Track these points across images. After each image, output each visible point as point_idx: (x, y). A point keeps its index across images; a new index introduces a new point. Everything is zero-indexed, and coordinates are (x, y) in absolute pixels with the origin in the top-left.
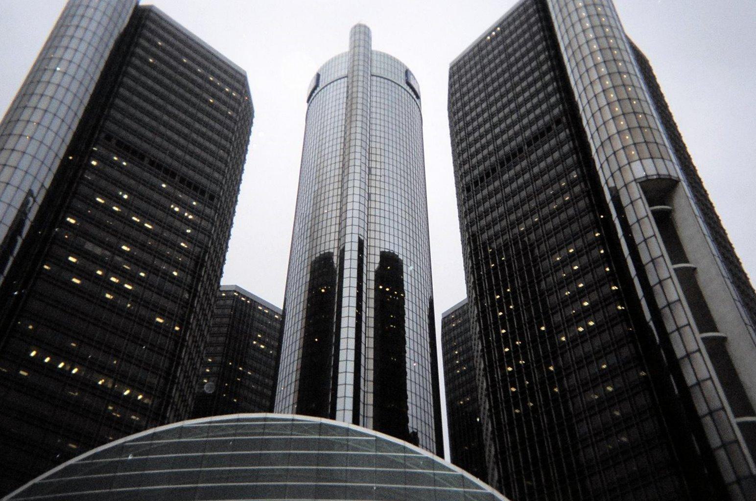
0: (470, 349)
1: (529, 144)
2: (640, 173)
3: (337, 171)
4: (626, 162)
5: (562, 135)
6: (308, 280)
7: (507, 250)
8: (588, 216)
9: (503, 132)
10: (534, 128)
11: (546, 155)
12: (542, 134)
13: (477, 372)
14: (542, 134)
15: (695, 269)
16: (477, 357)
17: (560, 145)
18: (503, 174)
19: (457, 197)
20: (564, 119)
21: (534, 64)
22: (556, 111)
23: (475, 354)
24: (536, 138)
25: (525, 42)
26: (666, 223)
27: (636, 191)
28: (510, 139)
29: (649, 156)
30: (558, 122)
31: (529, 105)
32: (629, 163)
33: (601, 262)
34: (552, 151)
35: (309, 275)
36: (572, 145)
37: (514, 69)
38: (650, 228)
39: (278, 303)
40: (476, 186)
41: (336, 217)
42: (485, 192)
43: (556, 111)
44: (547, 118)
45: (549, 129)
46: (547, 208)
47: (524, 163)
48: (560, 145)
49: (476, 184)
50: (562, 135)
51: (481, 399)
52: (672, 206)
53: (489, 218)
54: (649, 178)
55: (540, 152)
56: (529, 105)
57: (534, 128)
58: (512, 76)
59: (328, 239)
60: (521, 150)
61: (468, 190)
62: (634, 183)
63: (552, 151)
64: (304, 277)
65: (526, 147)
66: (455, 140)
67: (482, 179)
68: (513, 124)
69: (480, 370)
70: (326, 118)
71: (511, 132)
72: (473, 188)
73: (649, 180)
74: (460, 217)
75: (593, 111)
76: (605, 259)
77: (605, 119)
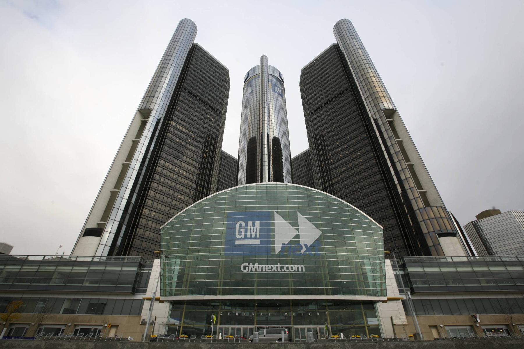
1: (335, 97)
49: (315, 111)
61: (312, 113)
67: (317, 110)
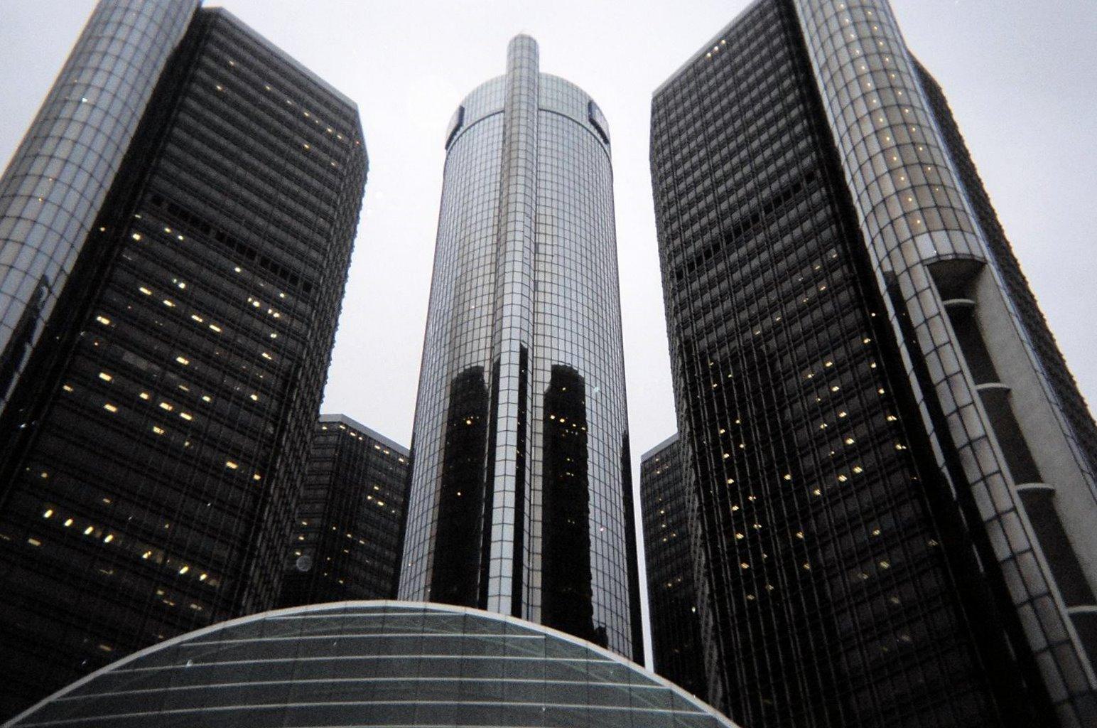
0: (682, 507)
1: (768, 209)
2: (928, 252)
3: (489, 249)
4: (908, 235)
5: (816, 197)
6: (447, 406)
7: (735, 363)
8: (853, 314)
9: (730, 192)
10: (775, 186)
11: (792, 226)
12: (787, 195)
13: (693, 540)
14: (787, 195)
15: (1008, 391)
16: (692, 518)
17: (813, 210)
18: (730, 252)
19: (664, 287)
20: (819, 174)
21: (775, 93)
22: (807, 162)
23: (690, 514)
24: (777, 201)
25: (763, 61)
26: (966, 324)
27: (923, 278)
28: (741, 203)
29: (942, 227)
30: (810, 177)
31: (768, 153)
32: (913, 238)
33: (872, 380)
34: (800, 220)
35: (448, 400)
36: (829, 211)
37: (746, 100)
38: (943, 331)
39: (403, 440)
40: (690, 271)
41: (488, 315)
42: (704, 279)
43: (807, 162)
44: (794, 171)
45: (796, 187)
46: (794, 302)
47: (761, 237)
48: (813, 210)
49: (691, 267)
50: (816, 197)
51: (698, 579)
52: (976, 299)
53: (710, 317)
54: (942, 258)
55: (783, 221)
56: (768, 153)
57: (775, 186)
58: (743, 110)
59: (475, 348)
60: (755, 218)
61: (680, 276)
62: (920, 266)
63: (800, 220)
64: (441, 402)
65: (763, 214)
66: (660, 203)
67: (699, 261)
68: (745, 180)
69: (696, 537)
70: (473, 172)
71: (741, 192)
72: (686, 273)
73: (941, 261)
74: (667, 315)
75: (861, 162)
76: (877, 377)
77: (879, 174)
